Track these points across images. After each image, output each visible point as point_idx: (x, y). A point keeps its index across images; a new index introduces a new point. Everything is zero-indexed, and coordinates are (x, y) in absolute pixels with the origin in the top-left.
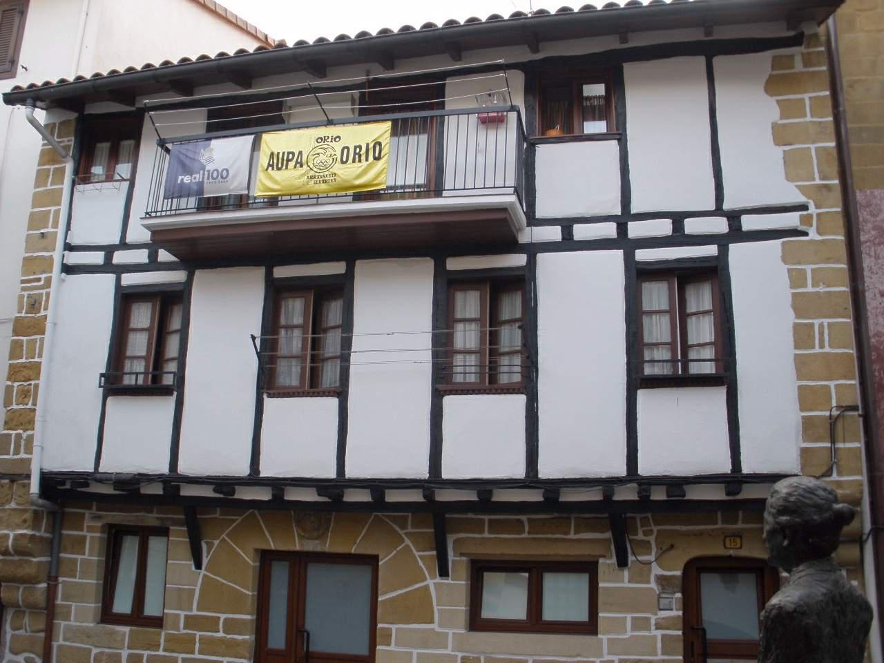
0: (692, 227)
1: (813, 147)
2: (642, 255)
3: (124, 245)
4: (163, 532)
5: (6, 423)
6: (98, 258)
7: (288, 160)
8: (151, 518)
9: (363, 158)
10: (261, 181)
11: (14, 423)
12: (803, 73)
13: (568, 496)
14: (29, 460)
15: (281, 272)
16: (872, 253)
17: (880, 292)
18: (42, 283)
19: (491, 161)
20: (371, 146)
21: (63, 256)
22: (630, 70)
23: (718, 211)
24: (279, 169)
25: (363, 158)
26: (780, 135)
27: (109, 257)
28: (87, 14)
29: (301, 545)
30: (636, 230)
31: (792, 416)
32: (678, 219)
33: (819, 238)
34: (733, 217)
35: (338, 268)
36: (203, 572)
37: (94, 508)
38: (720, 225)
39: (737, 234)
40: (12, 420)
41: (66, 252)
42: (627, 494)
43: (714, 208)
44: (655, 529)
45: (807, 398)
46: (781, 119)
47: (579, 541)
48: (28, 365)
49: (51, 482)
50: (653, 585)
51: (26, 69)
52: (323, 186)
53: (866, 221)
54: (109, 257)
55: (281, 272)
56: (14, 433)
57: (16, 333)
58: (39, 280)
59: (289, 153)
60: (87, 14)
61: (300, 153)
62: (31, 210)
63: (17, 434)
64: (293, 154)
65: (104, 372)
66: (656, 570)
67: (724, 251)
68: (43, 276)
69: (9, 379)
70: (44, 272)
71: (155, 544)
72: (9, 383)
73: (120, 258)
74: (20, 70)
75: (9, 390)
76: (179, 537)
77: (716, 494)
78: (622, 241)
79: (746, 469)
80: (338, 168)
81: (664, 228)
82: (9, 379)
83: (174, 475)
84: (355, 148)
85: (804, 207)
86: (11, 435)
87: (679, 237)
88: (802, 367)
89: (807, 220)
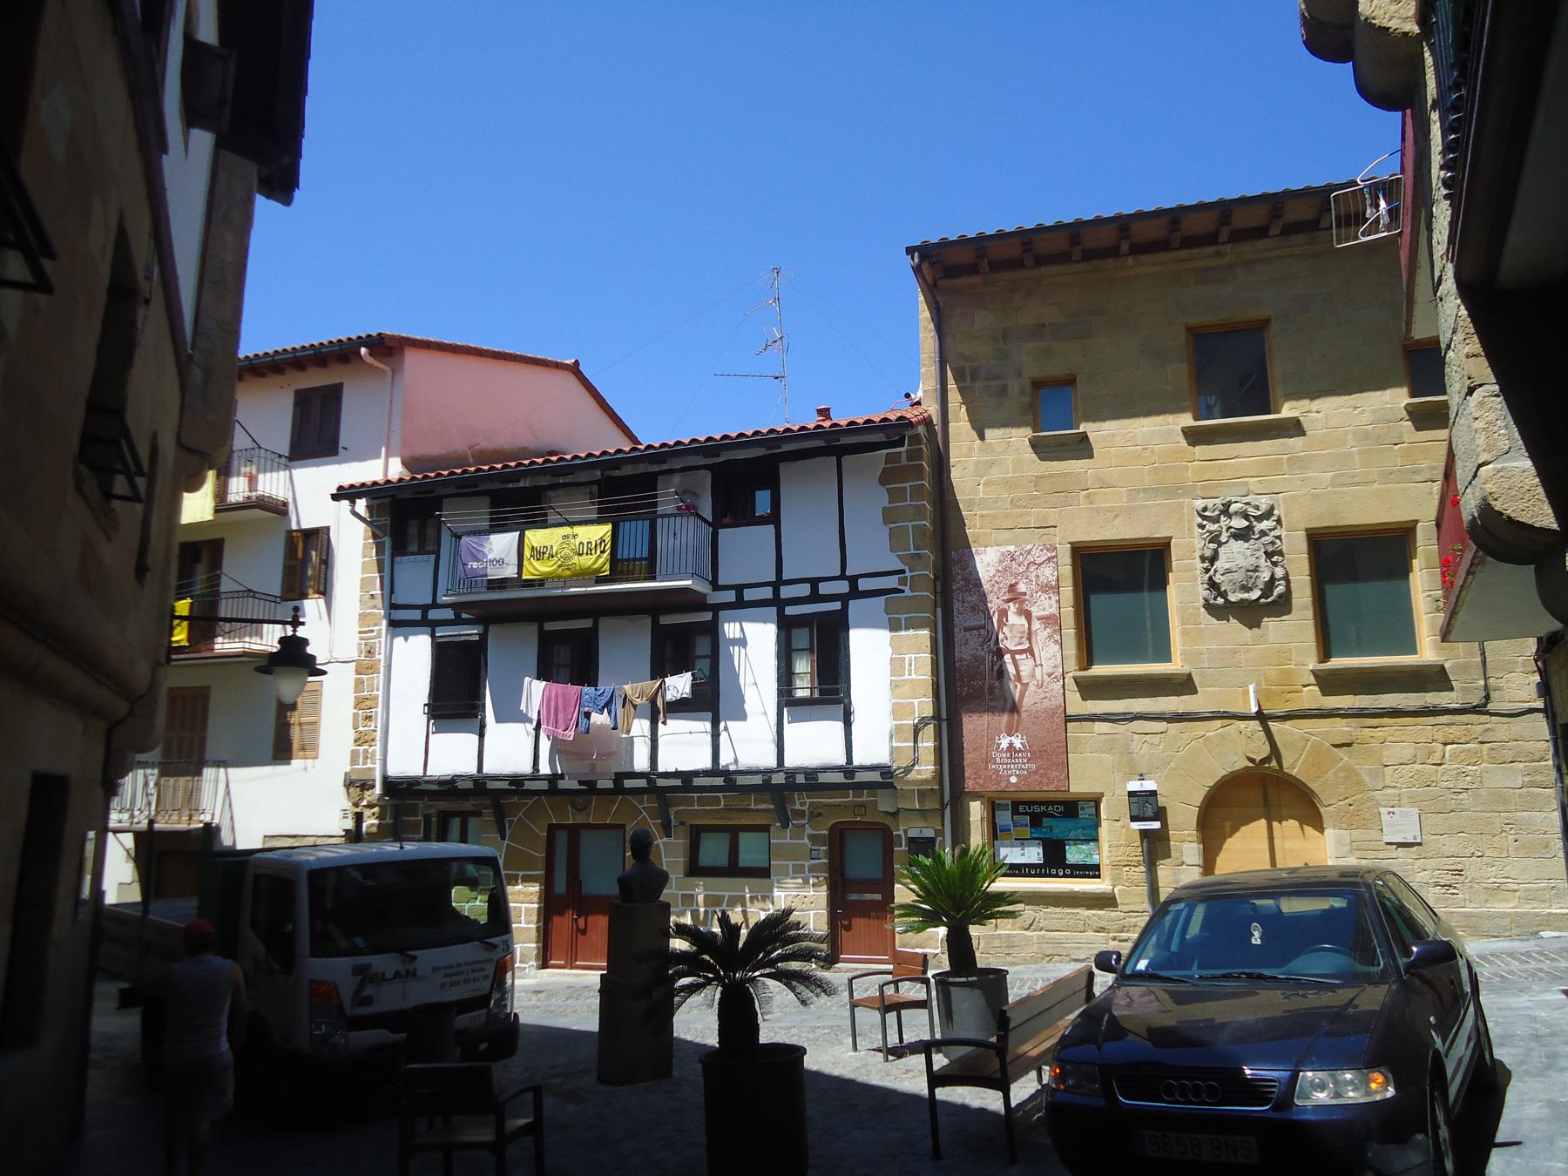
0: (824, 589)
1: (910, 524)
2: (790, 611)
3: (435, 605)
4: (477, 814)
5: (355, 741)
6: (416, 615)
7: (544, 553)
8: (468, 805)
9: (593, 551)
10: (527, 568)
11: (361, 741)
12: (907, 466)
13: (741, 780)
14: (374, 769)
15: (550, 626)
16: (960, 599)
17: (964, 628)
18: (375, 633)
19: (684, 543)
20: (598, 542)
21: (390, 614)
22: (785, 469)
23: (842, 577)
24: (538, 560)
25: (593, 551)
26: (888, 516)
27: (425, 615)
28: (391, 402)
29: (574, 820)
30: (786, 592)
31: (886, 724)
32: (814, 582)
33: (911, 594)
34: (853, 581)
35: (586, 623)
36: (506, 842)
37: (426, 800)
38: (843, 587)
39: (855, 593)
40: (360, 738)
41: (392, 611)
42: (778, 779)
43: (840, 573)
44: (808, 801)
45: (897, 711)
46: (889, 503)
47: (758, 810)
48: (369, 697)
49: (391, 785)
50: (806, 840)
51: (346, 449)
52: (568, 572)
53: (958, 574)
54: (425, 615)
55: (550, 626)
56: (361, 748)
57: (358, 673)
58: (372, 631)
59: (544, 547)
60: (391, 402)
61: (552, 547)
62: (361, 576)
63: (364, 750)
64: (547, 547)
65: (427, 702)
66: (808, 830)
67: (845, 607)
68: (376, 628)
69: (355, 708)
70: (376, 625)
71: (473, 822)
72: (356, 711)
73: (433, 615)
74: (341, 450)
75: (355, 715)
76: (489, 817)
77: (838, 778)
78: (778, 602)
79: (856, 762)
80: (576, 559)
81: (804, 590)
82: (355, 708)
83: (480, 775)
84: (588, 543)
85: (903, 572)
86: (359, 750)
87: (815, 597)
88: (894, 686)
89: (903, 581)
